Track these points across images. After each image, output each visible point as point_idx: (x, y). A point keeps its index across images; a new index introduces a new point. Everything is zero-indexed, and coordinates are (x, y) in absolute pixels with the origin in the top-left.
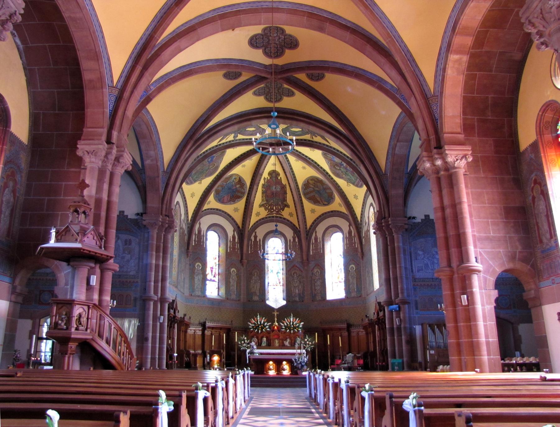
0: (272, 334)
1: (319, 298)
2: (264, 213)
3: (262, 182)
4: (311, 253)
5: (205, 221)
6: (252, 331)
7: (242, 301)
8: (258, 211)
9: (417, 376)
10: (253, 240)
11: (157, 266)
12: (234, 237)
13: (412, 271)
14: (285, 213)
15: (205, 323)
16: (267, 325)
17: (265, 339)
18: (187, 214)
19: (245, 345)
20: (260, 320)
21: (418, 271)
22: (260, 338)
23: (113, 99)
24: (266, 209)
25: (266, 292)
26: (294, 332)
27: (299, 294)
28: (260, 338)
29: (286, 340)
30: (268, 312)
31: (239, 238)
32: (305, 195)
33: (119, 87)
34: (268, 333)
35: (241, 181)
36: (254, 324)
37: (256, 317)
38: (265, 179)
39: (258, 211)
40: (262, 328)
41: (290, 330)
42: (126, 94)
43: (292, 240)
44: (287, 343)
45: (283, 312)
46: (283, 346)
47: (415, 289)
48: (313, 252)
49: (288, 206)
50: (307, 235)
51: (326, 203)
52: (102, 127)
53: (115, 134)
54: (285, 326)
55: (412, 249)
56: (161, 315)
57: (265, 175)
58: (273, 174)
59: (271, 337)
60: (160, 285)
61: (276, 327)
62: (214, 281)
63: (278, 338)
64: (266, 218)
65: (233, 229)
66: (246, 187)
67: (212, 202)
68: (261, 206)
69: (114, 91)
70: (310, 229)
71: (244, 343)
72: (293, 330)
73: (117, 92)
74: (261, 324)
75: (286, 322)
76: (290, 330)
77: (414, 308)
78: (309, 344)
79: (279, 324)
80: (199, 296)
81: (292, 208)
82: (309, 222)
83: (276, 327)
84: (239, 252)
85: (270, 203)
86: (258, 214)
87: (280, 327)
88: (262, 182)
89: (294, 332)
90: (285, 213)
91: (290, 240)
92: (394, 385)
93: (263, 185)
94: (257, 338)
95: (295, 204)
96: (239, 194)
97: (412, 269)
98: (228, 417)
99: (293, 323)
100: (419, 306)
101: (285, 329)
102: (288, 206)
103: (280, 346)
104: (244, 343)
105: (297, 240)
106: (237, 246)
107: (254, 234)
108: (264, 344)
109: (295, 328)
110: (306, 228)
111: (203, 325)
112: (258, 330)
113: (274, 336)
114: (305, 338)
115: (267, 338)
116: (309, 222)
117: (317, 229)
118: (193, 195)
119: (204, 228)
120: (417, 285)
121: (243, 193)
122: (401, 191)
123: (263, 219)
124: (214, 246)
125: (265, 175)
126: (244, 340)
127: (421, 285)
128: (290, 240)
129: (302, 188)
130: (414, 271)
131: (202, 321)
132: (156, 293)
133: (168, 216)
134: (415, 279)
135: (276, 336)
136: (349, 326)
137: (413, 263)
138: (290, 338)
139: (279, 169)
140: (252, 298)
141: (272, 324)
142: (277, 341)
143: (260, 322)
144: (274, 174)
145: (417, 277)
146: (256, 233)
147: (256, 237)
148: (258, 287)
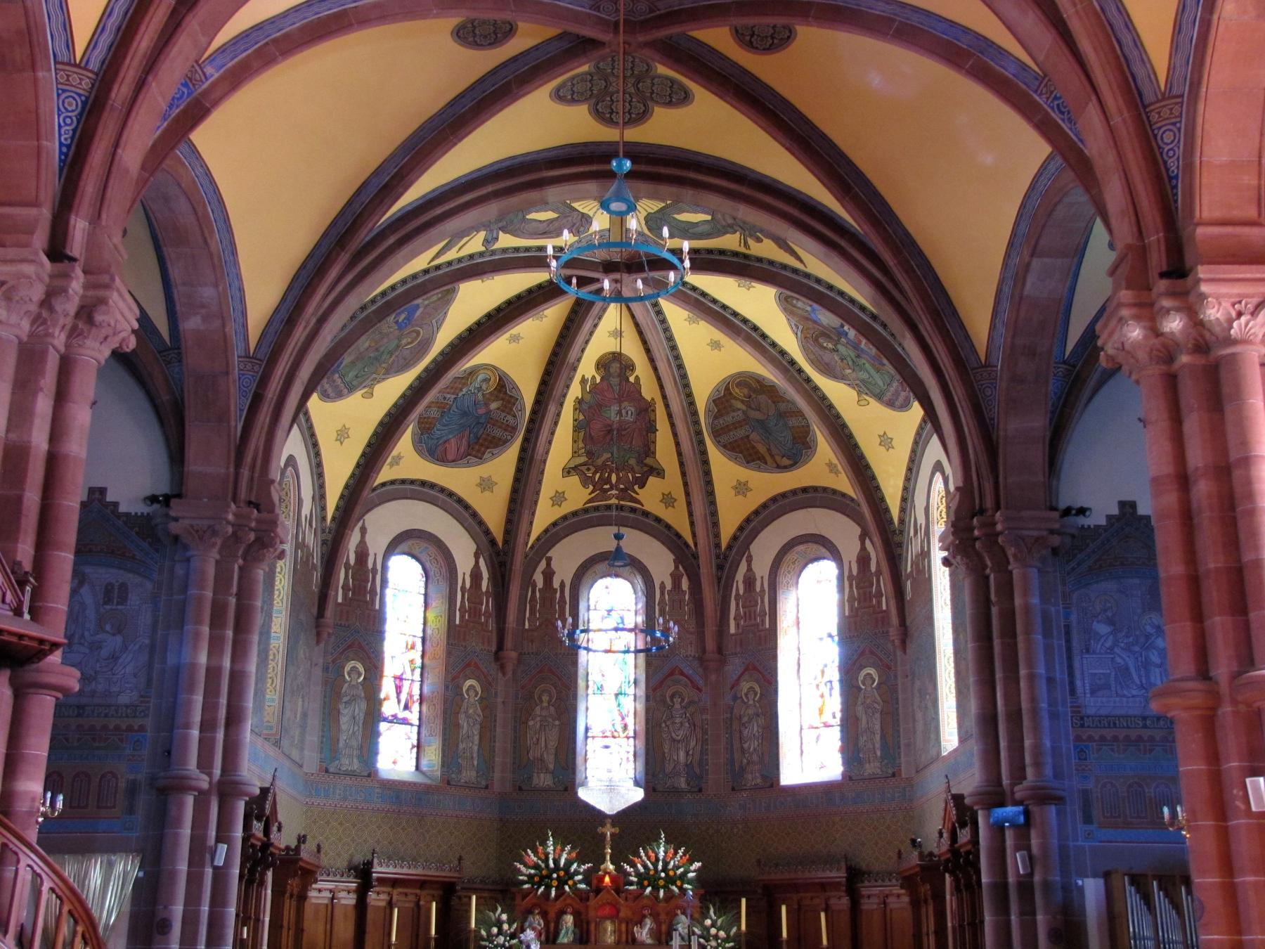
2: (578, 495)
3: (575, 391)
4: (732, 630)
5: (382, 523)
6: (528, 892)
8: (560, 492)
10: (540, 584)
11: (213, 673)
12: (476, 575)
13: (1073, 692)
14: (650, 496)
15: (369, 865)
16: (577, 873)
17: (569, 919)
18: (323, 497)
20: (556, 853)
21: (1093, 692)
22: (552, 915)
23: (74, 106)
24: (585, 481)
26: (670, 896)
28: (552, 915)
29: (640, 923)
31: (493, 578)
32: (716, 434)
33: (94, 65)
34: (582, 897)
35: (504, 388)
36: (536, 867)
38: (583, 381)
39: (560, 492)
40: (562, 882)
41: (656, 889)
42: (121, 91)
43: (669, 586)
45: (634, 827)
47: (1082, 754)
48: (737, 625)
49: (660, 473)
50: (720, 567)
51: (786, 462)
52: (35, 204)
53: (79, 226)
54: (638, 874)
55: (1074, 618)
56: (219, 840)
57: (587, 368)
58: (614, 364)
59: (592, 913)
60: (220, 735)
61: (607, 879)
62: (405, 722)
63: (614, 917)
64: (586, 511)
65: (473, 547)
66: (523, 409)
67: (406, 459)
68: (567, 472)
69: (75, 79)
70: (729, 547)
73: (86, 84)
75: (643, 861)
76: (656, 889)
77: (1079, 815)
78: (716, 937)
79: (619, 869)
80: (352, 774)
81: (672, 481)
82: (728, 528)
83: (607, 879)
84: (492, 625)
85: (599, 462)
86: (558, 498)
87: (620, 879)
88: (575, 391)
89: (670, 896)
90: (650, 496)
91: (663, 586)
93: (579, 402)
94: (544, 915)
95: (682, 464)
96: (498, 433)
97: (1072, 683)
99: (666, 864)
100: (1096, 813)
101: (640, 883)
102: (660, 473)
104: (500, 932)
105: (685, 584)
106: (487, 605)
107: (543, 564)
109: (670, 880)
110: (718, 546)
111: (363, 873)
112: (548, 888)
114: (705, 915)
116: (728, 528)
117: (754, 548)
118: (342, 435)
119: (377, 545)
120: (1090, 738)
121: (513, 430)
122: (1038, 422)
123: (575, 514)
124: (407, 603)
125: (587, 368)
126: (499, 924)
127: (1103, 738)
128: (663, 586)
129: (708, 411)
130: (1079, 690)
131: (359, 859)
132: (205, 764)
133: (257, 506)
134: (1081, 719)
136: (855, 876)
137: (1077, 664)
138: (655, 916)
139: (632, 349)
140: (530, 778)
141: (596, 869)
142: (609, 927)
143: (556, 861)
144: (615, 367)
145: (1091, 711)
146: (549, 560)
147: (549, 575)
148: (553, 744)
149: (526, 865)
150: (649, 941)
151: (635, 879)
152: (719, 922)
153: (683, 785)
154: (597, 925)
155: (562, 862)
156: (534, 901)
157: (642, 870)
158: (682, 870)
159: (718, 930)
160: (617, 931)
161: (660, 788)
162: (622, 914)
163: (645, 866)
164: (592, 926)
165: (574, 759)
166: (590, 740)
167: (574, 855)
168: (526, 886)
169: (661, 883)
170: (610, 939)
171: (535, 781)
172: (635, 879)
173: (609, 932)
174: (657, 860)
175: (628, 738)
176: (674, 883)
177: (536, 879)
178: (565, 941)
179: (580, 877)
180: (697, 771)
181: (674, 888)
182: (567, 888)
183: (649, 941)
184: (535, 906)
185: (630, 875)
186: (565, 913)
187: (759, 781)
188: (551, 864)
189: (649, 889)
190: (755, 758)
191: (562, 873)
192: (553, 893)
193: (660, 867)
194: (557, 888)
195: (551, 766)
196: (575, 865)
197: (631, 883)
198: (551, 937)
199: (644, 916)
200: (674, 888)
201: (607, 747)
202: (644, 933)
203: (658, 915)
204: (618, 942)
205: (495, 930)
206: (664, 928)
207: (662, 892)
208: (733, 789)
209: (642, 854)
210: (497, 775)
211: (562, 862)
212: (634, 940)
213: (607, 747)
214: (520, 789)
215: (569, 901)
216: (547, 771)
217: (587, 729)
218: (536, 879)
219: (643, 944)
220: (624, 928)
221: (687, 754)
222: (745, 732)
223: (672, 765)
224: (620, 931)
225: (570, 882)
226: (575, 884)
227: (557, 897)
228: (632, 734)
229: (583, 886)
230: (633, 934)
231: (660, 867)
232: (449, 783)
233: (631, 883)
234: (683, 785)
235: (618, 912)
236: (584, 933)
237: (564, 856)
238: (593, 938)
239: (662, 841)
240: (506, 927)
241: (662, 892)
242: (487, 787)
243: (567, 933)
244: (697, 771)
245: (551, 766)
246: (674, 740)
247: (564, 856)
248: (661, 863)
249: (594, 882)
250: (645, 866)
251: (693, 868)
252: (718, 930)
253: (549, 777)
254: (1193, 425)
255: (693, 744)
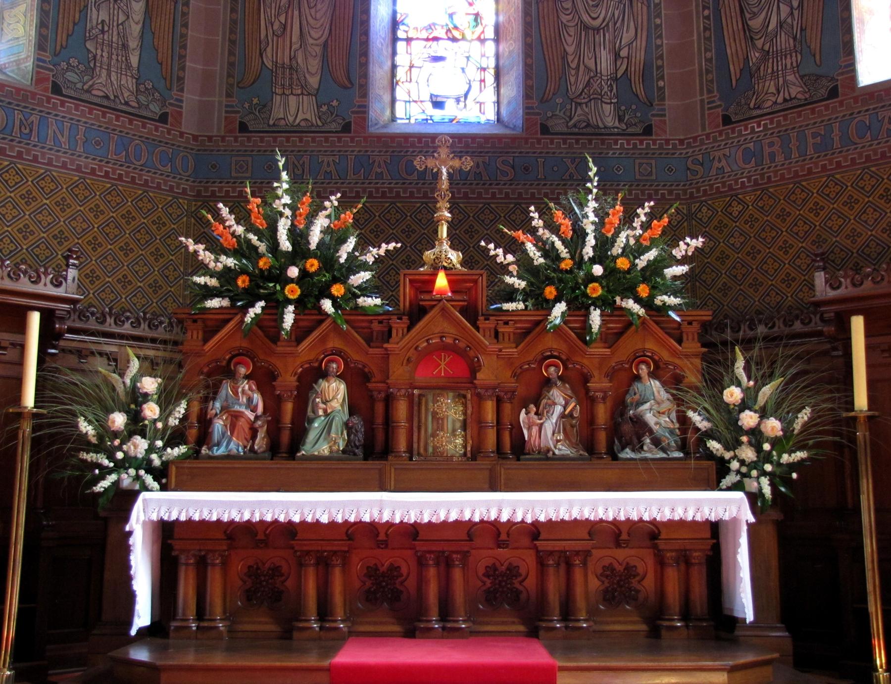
1: (782, 84)
6: (221, 319)
7: (189, 125)
9: (405, 413)
16: (353, 265)
17: (335, 392)
19: (139, 446)
20: (301, 217)
22: (288, 380)
25: (378, 73)
26: (620, 326)
27: (620, 80)
28: (288, 380)
29: (536, 398)
30: (392, 182)
34: (375, 331)
36: (244, 250)
37: (266, 192)
40: (312, 291)
41: (579, 307)
44: (547, 428)
45: (503, 176)
46: (506, 459)
54: (526, 266)
59: (399, 372)
61: (442, 281)
63: (465, 384)
71: (136, 425)
72: (605, 303)
74: (300, 250)
75: (540, 239)
76: (579, 307)
78: (756, 434)
79: (475, 258)
83: (442, 281)
87: (476, 298)
89: (620, 326)
94: (265, 380)
99: (604, 244)
101: (533, 294)
103: (475, 453)
104: (136, 425)
108: (323, 440)
109: (619, 282)
112: (276, 306)
113: (428, 355)
114: (716, 382)
126: (135, 400)
135: (443, 366)
138: (579, 384)
140: (265, 107)
141: (410, 257)
143: (298, 236)
148: (317, 35)
149: (216, 248)
151: (521, 284)
152: (767, 391)
153: (610, 121)
154: (415, 405)
155: (315, 237)
156: (240, 343)
157: (539, 259)
158: (652, 254)
159: (764, 414)
160: (472, 424)
161: (558, 125)
163: (549, 252)
164: (401, 409)
165: (364, 65)
166: (401, 46)
167: (348, 217)
168: (214, 303)
169: (595, 290)
171: (277, 112)
172: (521, 284)
174: (580, 234)
175: (482, 41)
176: (630, 291)
177: (242, 282)
178: (324, 449)
179: (364, 276)
180: (640, 89)
181: (630, 304)
182: (327, 305)
183: (563, 450)
184: (239, 355)
185: (504, 269)
186: (324, 375)
187: (794, 91)
188: (286, 245)
189: (560, 308)
190: (784, 41)
191: (313, 265)
192: (289, 318)
193: (588, 251)
194: (299, 304)
195: (314, 81)
196: (351, 244)
197: (510, 294)
198: (285, 437)
199: (547, 383)
200: (630, 304)
201: (437, 59)
203: (585, 379)
205: (119, 420)
206: (602, 413)
207: (595, 318)
208: (727, 120)
209: (537, 222)
210: (190, 98)
211: (315, 237)
213: (437, 59)
214: (243, 128)
215: (334, 343)
216: (305, 90)
217: (395, 24)
218: (242, 282)
221: (617, 56)
222: (606, 220)
223: (583, 79)
224: (480, 423)
225: (337, 290)
226: (352, 294)
227: (300, 332)
228: (490, 33)
229: (371, 302)
231: (588, 251)
232: (57, 89)
233: (510, 294)
234: (610, 121)
235: (474, 369)
237: (321, 222)
238: (402, 445)
239: (592, 186)
240: (151, 411)
242: (163, 118)
243: (328, 426)
244: (640, 89)
245: (314, 81)
246: (587, 28)
247: (321, 222)
249: (406, 292)
250: (549, 252)
251: (679, 252)
252: (764, 414)
253: (308, 102)
255: (627, 37)
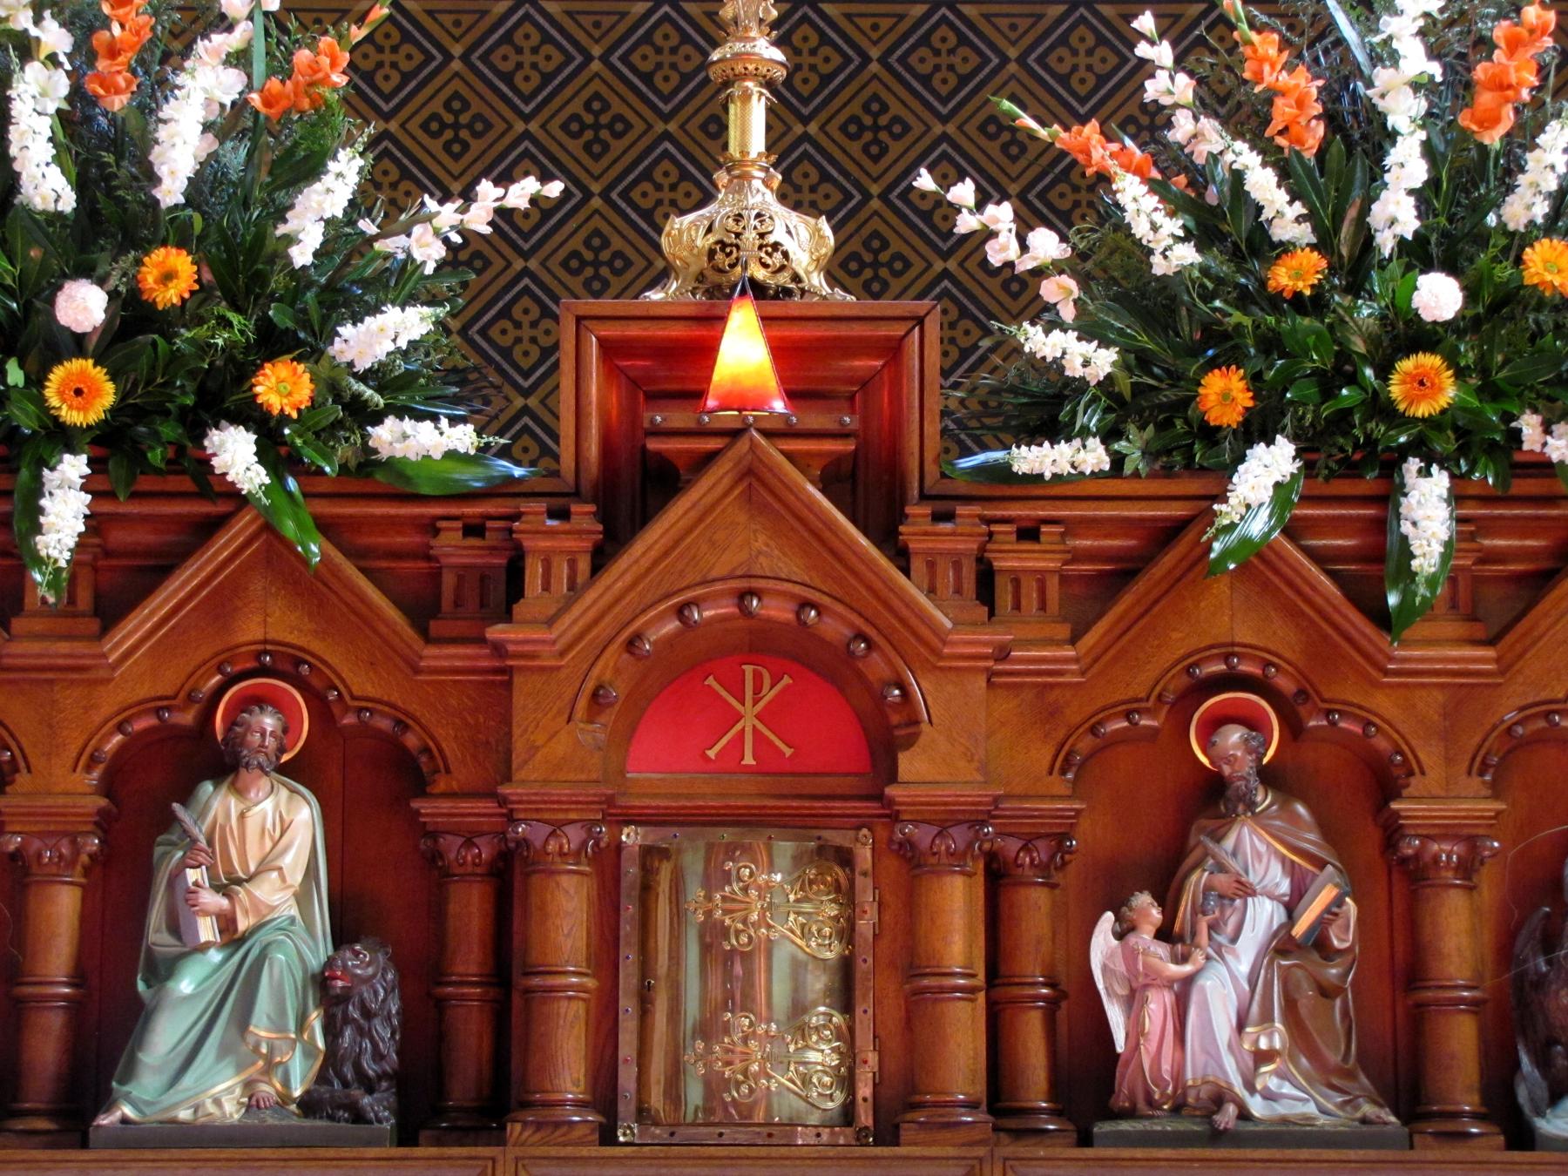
0: (566, 618)
17: (270, 838)
29: (1162, 865)
34: (448, 566)
40: (169, 393)
41: (1354, 460)
54: (1118, 282)
59: (556, 750)
61: (743, 352)
63: (845, 799)
72: (1466, 443)
74: (113, 215)
76: (1354, 460)
79: (888, 245)
83: (743, 352)
92: (142, 1164)
98: (639, 1066)
101: (1152, 405)
113: (683, 675)
115: (367, 781)
138: (1357, 802)
141: (603, 239)
142: (785, 918)
150: (1286, 1096)
154: (626, 902)
155: (179, 153)
157: (1173, 252)
160: (879, 980)
162: (922, 770)
164: (566, 915)
170: (800, 1069)
173: (771, 984)
174: (1359, 138)
178: (219, 1094)
182: (235, 453)
183: (1286, 1096)
185: (1020, 293)
186: (225, 765)
189: (1269, 467)
191: (171, 275)
193: (1396, 214)
194: (111, 445)
197: (1047, 407)
199: (1212, 798)
202: (1214, 995)
203: (1383, 780)
204: (893, 1109)
207: (1428, 509)
209: (1169, 85)
211: (179, 153)
212: (1090, 1083)
215: (269, 621)
219: (1205, 1118)
220: (957, 939)
225: (282, 387)
227: (116, 574)
229: (421, 440)
230: (1076, 1004)
231: (1396, 214)
233: (1047, 407)
235: (885, 736)
236: (450, 1020)
241: (1428, 509)
243: (238, 995)
248: (1407, 165)
250: (1220, 219)
254: (468, 961)
